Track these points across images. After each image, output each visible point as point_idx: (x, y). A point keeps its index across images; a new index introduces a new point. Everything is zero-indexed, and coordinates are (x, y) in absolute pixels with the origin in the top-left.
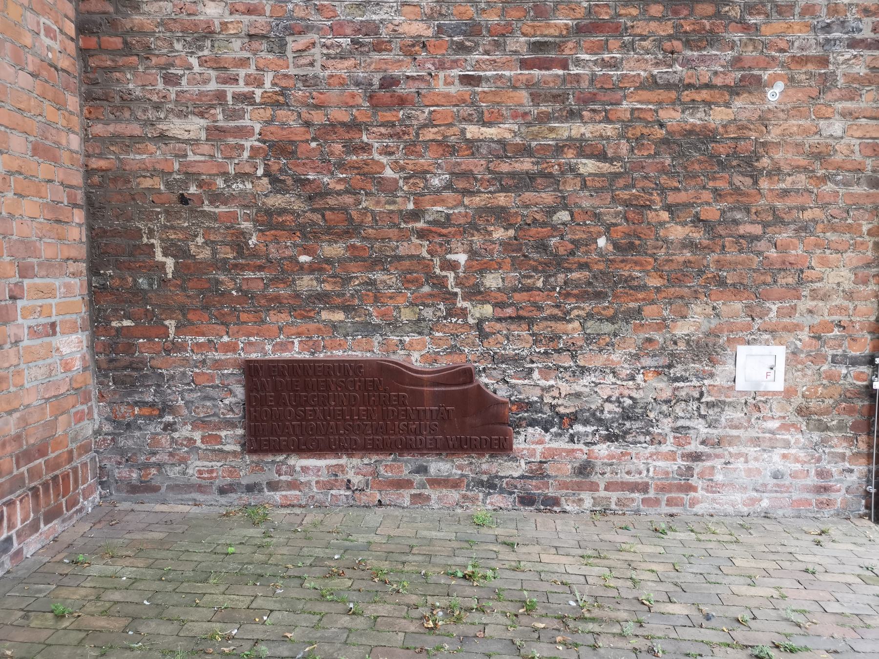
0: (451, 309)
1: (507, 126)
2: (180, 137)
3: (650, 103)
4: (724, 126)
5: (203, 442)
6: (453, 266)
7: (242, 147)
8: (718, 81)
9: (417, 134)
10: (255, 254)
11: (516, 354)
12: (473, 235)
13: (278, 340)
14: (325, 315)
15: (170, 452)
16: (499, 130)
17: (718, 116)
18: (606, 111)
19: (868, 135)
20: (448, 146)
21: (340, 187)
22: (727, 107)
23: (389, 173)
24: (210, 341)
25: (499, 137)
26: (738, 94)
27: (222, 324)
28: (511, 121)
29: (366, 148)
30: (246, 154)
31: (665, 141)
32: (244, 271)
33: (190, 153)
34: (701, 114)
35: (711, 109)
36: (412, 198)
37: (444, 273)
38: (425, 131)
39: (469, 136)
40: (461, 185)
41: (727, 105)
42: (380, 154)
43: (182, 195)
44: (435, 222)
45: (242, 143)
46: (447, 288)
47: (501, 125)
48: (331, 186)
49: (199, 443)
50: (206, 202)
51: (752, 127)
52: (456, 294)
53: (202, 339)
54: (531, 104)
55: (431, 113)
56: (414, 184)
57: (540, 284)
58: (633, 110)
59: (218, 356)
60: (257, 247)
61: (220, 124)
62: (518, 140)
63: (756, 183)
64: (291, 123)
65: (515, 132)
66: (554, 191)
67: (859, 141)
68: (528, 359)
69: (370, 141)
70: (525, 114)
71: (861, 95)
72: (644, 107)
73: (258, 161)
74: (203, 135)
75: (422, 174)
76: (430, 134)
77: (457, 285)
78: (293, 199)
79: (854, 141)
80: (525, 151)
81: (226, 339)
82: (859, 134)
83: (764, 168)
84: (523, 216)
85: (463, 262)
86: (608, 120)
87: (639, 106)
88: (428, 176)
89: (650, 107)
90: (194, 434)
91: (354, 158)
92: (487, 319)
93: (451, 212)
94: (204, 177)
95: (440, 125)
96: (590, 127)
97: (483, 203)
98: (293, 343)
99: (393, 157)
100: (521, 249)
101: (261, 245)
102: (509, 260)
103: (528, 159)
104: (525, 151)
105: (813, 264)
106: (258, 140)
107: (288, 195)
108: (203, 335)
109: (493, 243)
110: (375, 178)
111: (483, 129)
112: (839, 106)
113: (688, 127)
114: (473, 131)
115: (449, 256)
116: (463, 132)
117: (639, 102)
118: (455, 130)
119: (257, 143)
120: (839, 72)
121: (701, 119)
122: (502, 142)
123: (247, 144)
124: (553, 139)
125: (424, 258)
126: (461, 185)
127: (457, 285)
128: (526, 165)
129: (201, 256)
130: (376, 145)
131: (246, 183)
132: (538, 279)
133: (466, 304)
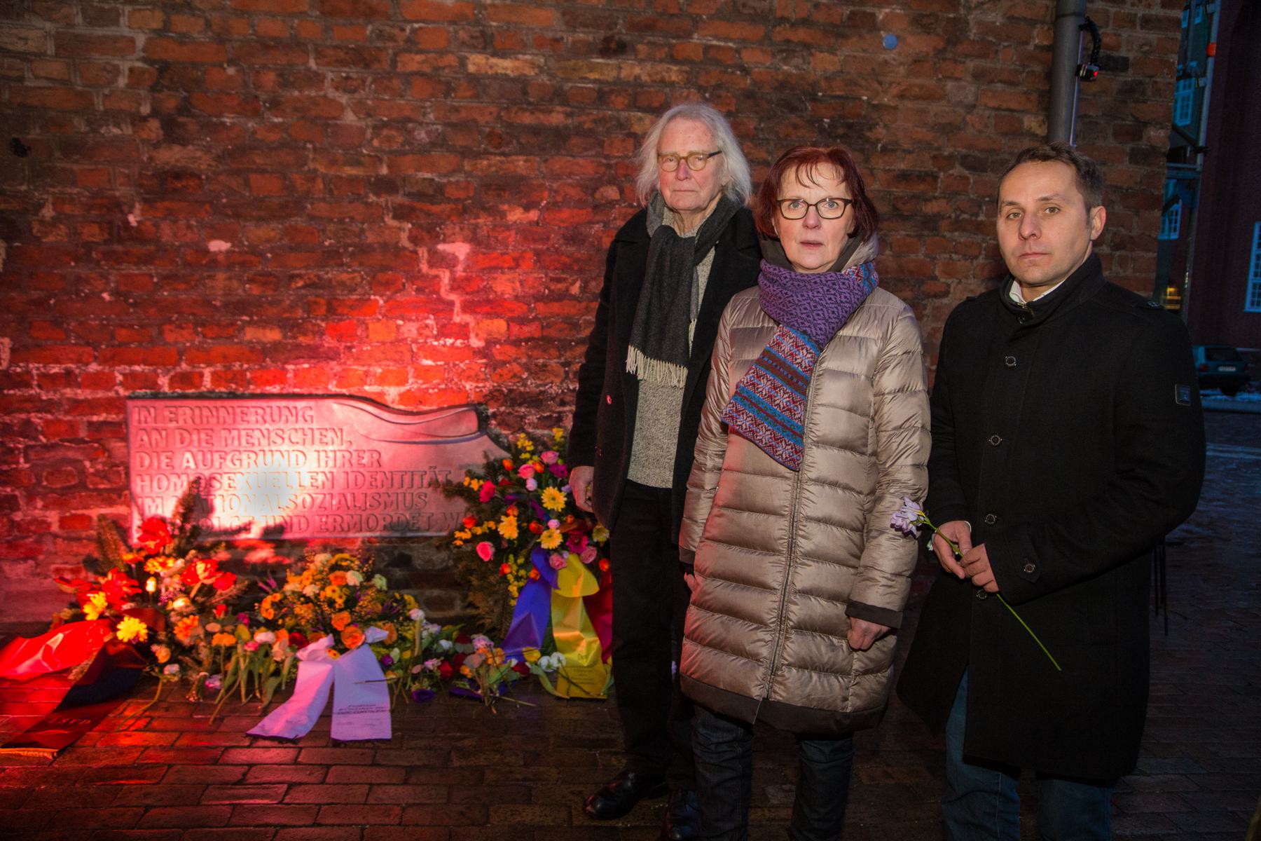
0: (444, 326)
1: (528, 57)
2: (10, 47)
3: (727, 39)
4: (827, 79)
5: (62, 526)
6: (448, 262)
7: (116, 71)
8: (820, 17)
9: (394, 63)
10: (137, 235)
11: (541, 392)
12: (477, 217)
13: (178, 370)
14: (250, 334)
15: (9, 542)
16: (517, 64)
17: (823, 64)
18: (671, 46)
19: (1004, 106)
20: (440, 82)
21: (273, 137)
22: (833, 54)
23: (350, 118)
24: (69, 373)
25: (516, 73)
26: (845, 37)
27: (88, 344)
28: (535, 51)
29: (315, 79)
30: (122, 82)
31: (749, 95)
32: (120, 263)
33: (28, 75)
34: (797, 61)
35: (811, 54)
36: (385, 158)
37: (434, 272)
38: (405, 57)
39: (471, 69)
40: (460, 141)
41: (832, 51)
42: (337, 89)
43: (17, 141)
44: (420, 196)
45: (116, 62)
46: (438, 293)
47: (520, 56)
48: (259, 136)
49: (55, 528)
50: (57, 154)
51: (863, 83)
52: (452, 303)
53: (55, 369)
54: (564, 28)
55: (414, 31)
56: (389, 139)
57: (575, 289)
58: (708, 48)
59: (83, 394)
60: (143, 227)
61: (78, 31)
62: (544, 78)
63: (867, 160)
64: (196, 35)
65: (539, 67)
66: (598, 155)
67: (993, 113)
68: (558, 400)
69: (322, 70)
70: (557, 41)
71: (997, 51)
72: (722, 44)
73: (141, 92)
74: (51, 50)
75: (402, 124)
76: (413, 62)
77: (453, 289)
78: (199, 154)
79: (987, 113)
80: (558, 96)
81: (94, 367)
82: (993, 103)
83: (878, 140)
84: (551, 190)
85: (462, 257)
86: (673, 60)
87: (715, 43)
88: (410, 125)
89: (731, 44)
90: (47, 513)
91: (296, 93)
92: (497, 341)
93: (445, 180)
94: (53, 114)
95: (429, 52)
96: (648, 66)
97: (493, 169)
98: (201, 375)
99: (357, 96)
100: (548, 238)
101: (148, 223)
102: (530, 255)
103: (559, 108)
104: (558, 96)
105: (937, 273)
106: (144, 60)
107: (190, 147)
108: (57, 361)
109: (508, 228)
110: (328, 125)
111: (494, 61)
112: (971, 64)
113: (780, 77)
114: (477, 62)
115: (441, 247)
116: (463, 62)
117: (717, 38)
118: (451, 60)
119: (139, 64)
120: (970, 17)
121: (797, 67)
122: (522, 82)
123: (125, 66)
124: (595, 81)
125: (404, 248)
126: (460, 141)
127: (453, 289)
128: (557, 118)
129: (51, 239)
130: (330, 75)
131: (123, 126)
132: (573, 284)
133: (468, 318)
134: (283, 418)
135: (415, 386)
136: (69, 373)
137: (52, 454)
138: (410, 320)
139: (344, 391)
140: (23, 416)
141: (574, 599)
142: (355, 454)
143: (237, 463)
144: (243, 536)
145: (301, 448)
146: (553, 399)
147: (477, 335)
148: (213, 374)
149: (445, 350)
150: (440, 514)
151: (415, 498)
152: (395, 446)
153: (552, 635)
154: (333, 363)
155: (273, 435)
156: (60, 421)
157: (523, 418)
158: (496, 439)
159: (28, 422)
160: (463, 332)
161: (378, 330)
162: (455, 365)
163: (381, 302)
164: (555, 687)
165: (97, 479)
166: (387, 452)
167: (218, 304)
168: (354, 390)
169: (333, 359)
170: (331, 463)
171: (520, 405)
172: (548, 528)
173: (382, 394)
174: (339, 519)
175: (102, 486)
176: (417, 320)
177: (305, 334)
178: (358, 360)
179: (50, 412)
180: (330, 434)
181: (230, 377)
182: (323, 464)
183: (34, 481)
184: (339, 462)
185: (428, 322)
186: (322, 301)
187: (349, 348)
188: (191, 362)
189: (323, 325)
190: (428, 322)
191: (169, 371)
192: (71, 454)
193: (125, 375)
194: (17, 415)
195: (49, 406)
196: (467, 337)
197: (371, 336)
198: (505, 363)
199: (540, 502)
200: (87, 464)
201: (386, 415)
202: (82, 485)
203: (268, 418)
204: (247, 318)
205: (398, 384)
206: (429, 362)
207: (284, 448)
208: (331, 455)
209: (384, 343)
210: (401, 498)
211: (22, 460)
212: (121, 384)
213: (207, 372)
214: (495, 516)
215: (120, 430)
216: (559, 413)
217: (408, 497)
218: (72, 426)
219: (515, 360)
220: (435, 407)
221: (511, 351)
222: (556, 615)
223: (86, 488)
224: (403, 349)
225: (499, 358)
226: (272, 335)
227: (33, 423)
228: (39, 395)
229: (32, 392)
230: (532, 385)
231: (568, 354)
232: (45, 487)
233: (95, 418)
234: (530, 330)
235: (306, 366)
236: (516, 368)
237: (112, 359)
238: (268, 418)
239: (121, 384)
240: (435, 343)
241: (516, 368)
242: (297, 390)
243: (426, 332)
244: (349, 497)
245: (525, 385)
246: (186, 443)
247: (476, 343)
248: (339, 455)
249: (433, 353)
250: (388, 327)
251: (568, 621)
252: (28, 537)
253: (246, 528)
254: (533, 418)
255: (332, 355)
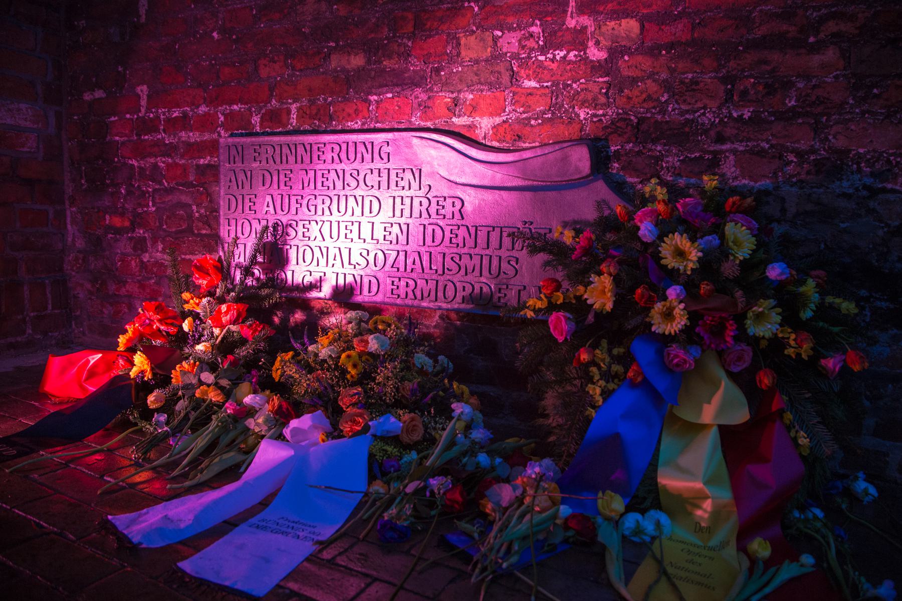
24: (185, 115)
59: (194, 137)
68: (712, 133)
92: (625, 50)
98: (289, 112)
133: (586, 21)
134: (359, 156)
135: (513, 116)
136: (185, 115)
137: (170, 197)
138: (511, 29)
139: (429, 124)
140: (152, 160)
141: (704, 427)
142: (434, 201)
143: (312, 208)
144: (314, 294)
145: (377, 194)
146: (706, 132)
147: (597, 43)
148: (299, 109)
149: (554, 66)
150: (528, 284)
151: (504, 265)
152: (488, 196)
153: (654, 479)
154: (418, 91)
155: (347, 176)
156: (177, 164)
157: (659, 159)
158: (618, 187)
159: (155, 166)
160: (579, 39)
161: (472, 47)
162: (566, 86)
163: (476, 9)
164: (628, 577)
165: (200, 224)
166: (471, 199)
167: (307, 31)
168: (439, 123)
169: (418, 85)
170: (407, 212)
171: (655, 141)
172: (665, 298)
173: (472, 127)
174: (411, 283)
175: (204, 232)
176: (519, 28)
177: (390, 57)
178: (446, 84)
179: (169, 156)
180: (408, 175)
181: (314, 112)
182: (398, 213)
183: (158, 224)
184: (416, 213)
185: (534, 29)
186: (410, 16)
187: (437, 70)
188: (280, 99)
189: (410, 44)
190: (534, 29)
191: (261, 109)
192: (185, 199)
193: (226, 116)
194: (148, 159)
195: (170, 150)
196: (583, 47)
197: (463, 53)
198: (634, 81)
199: (657, 257)
200: (194, 207)
201: (473, 152)
202: (190, 230)
203: (343, 156)
204: (333, 44)
205: (491, 115)
206: (533, 84)
207: (359, 192)
208: (407, 201)
209: (477, 62)
210: (485, 261)
211: (151, 204)
212: (223, 125)
213: (294, 108)
214: (582, 277)
215: (213, 171)
216: (715, 153)
217: (495, 262)
218: (185, 168)
219: (651, 76)
220: (537, 144)
221: (646, 63)
222: (668, 444)
223: (193, 232)
224: (501, 67)
225: (626, 73)
226: (357, 61)
227: (159, 167)
228: (163, 138)
229: (160, 136)
230: (674, 112)
231: (732, 64)
232: (164, 230)
233: (202, 161)
234: (678, 30)
235: (390, 95)
236: (652, 87)
237: (214, 101)
238: (343, 156)
239: (223, 125)
240: (542, 58)
241: (652, 87)
242: (379, 125)
243: (531, 43)
244: (425, 258)
245: (663, 112)
246: (267, 185)
247: (596, 54)
248: (416, 202)
249: (538, 72)
250: (482, 40)
251: (685, 461)
252: (151, 278)
253: (316, 285)
254: (673, 160)
255: (417, 82)
